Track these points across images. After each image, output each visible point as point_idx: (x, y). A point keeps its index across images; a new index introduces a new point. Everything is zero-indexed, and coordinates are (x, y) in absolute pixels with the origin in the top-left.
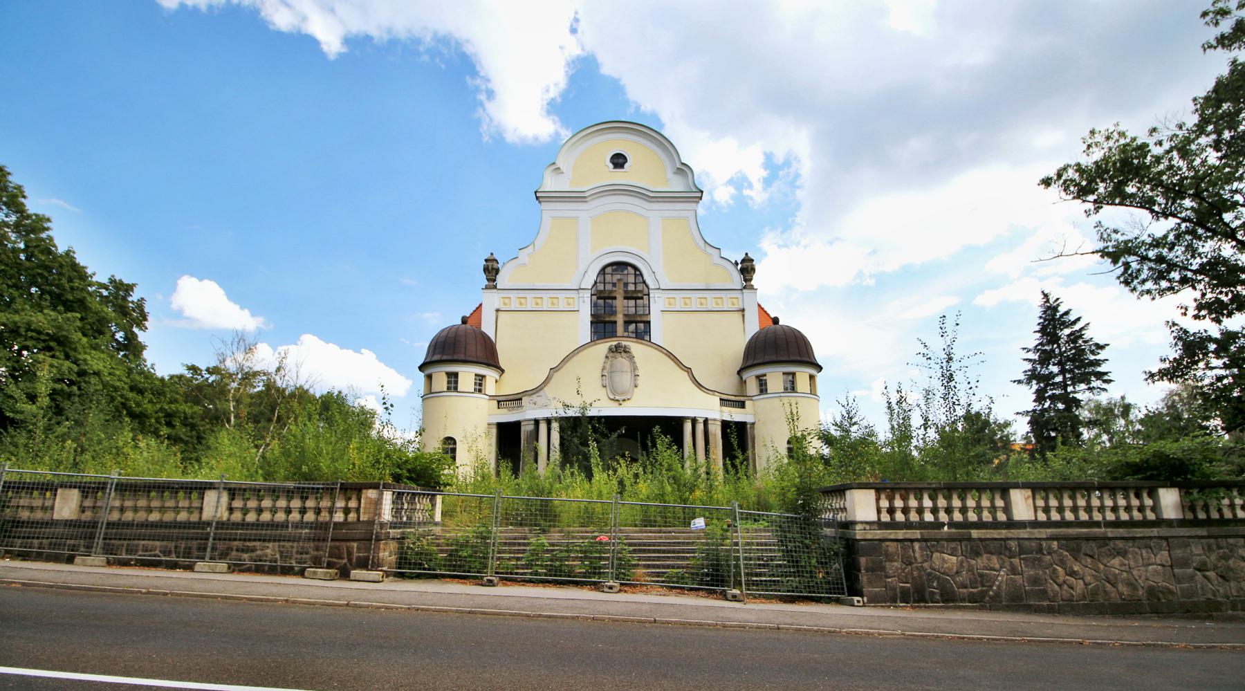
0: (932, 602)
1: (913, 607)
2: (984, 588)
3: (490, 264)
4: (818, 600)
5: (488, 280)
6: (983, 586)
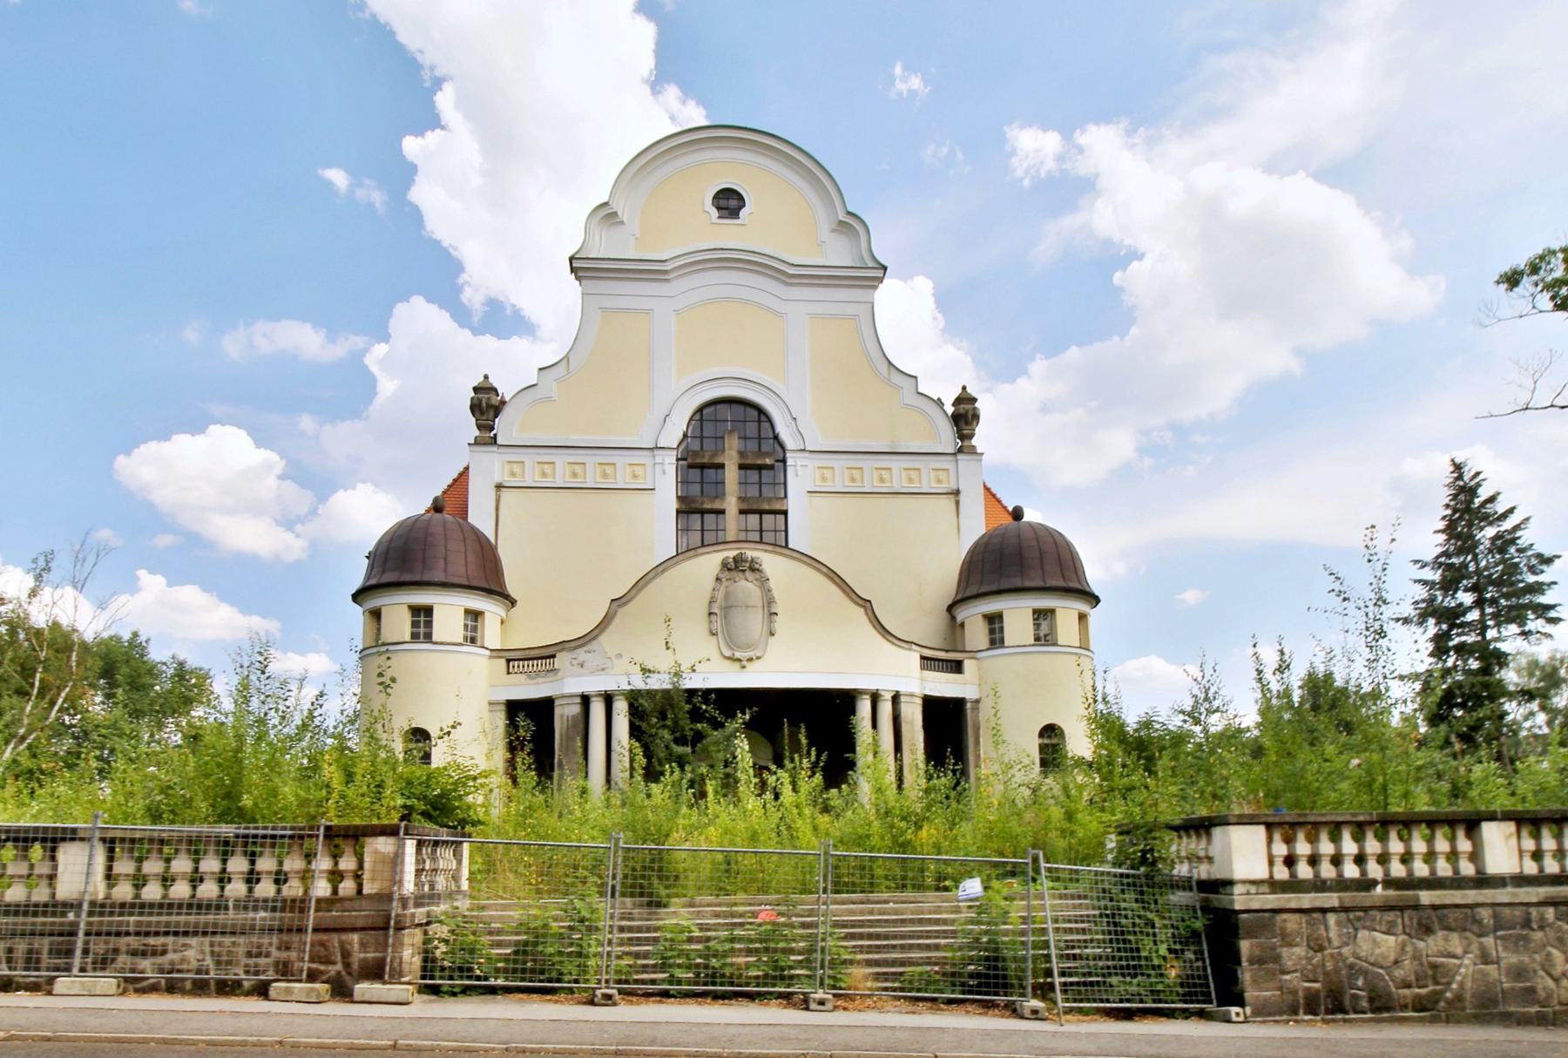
0: (1356, 1012)
1: (1325, 1021)
2: (1438, 987)
3: (483, 396)
4: (1170, 1014)
5: (479, 427)
6: (1437, 983)
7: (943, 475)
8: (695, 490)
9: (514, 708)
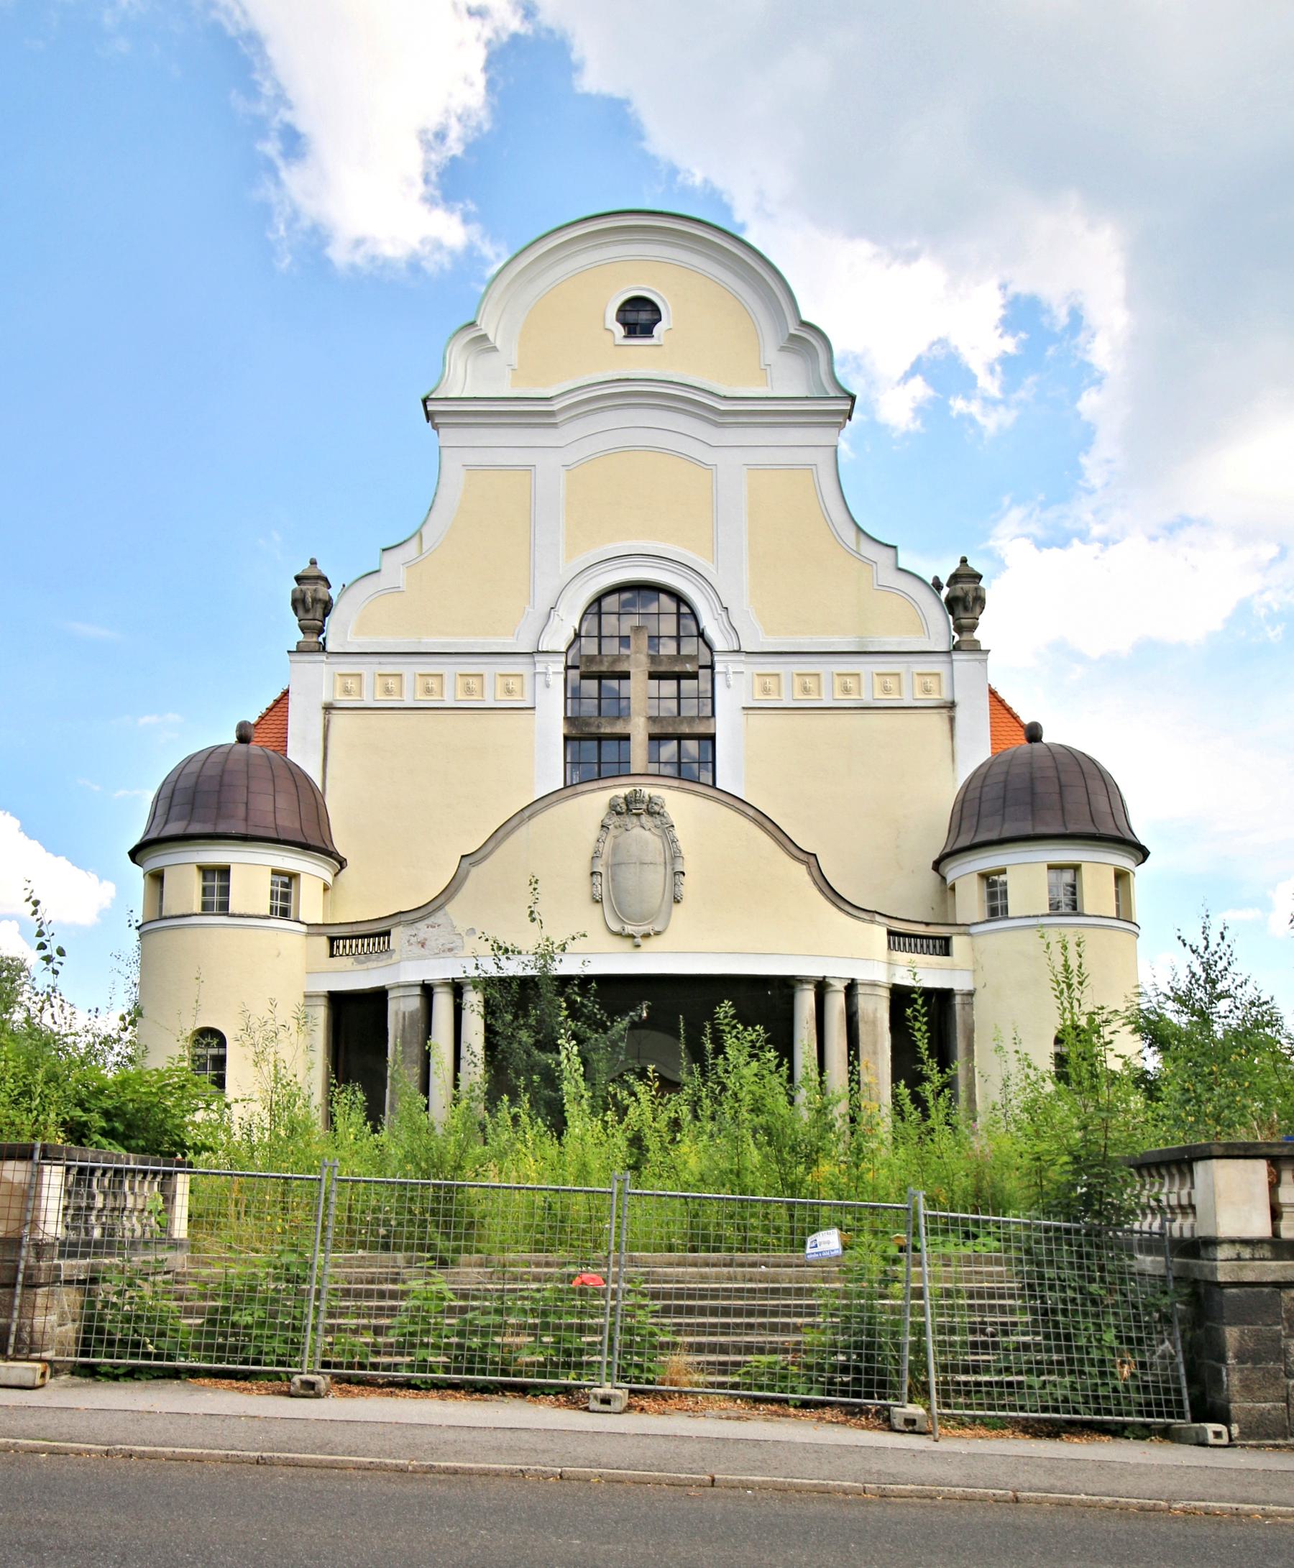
3: (308, 588)
4: (1117, 1431)
5: (304, 629)
7: (932, 682)
8: (589, 707)
9: (338, 1001)
